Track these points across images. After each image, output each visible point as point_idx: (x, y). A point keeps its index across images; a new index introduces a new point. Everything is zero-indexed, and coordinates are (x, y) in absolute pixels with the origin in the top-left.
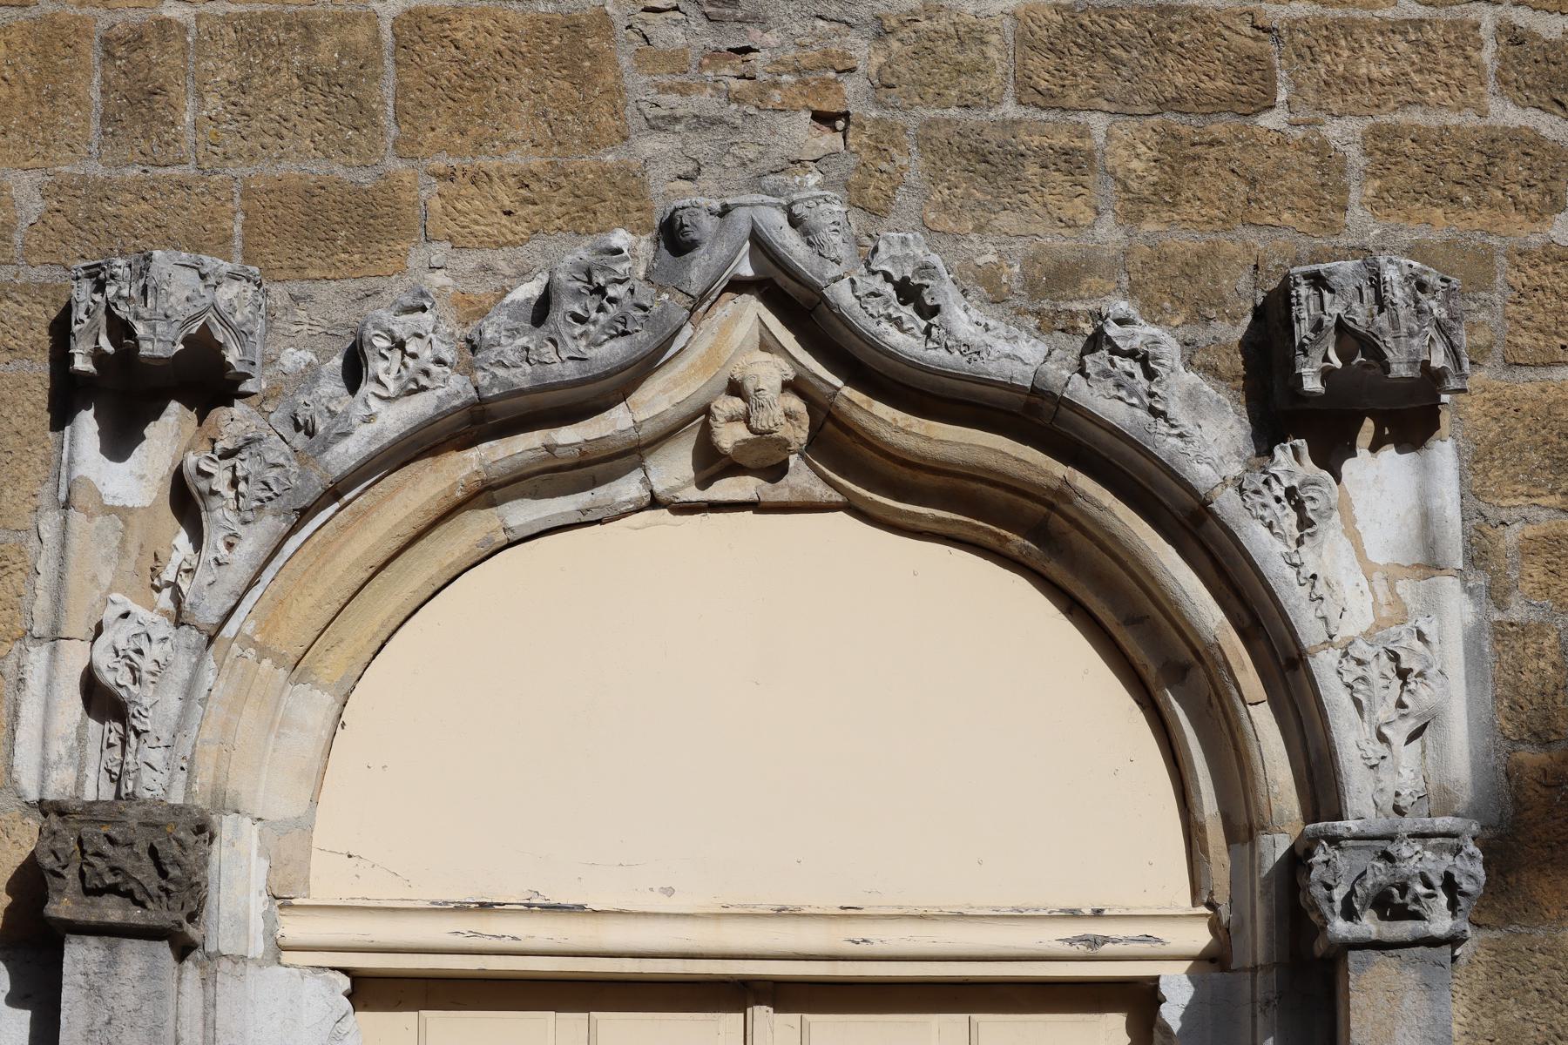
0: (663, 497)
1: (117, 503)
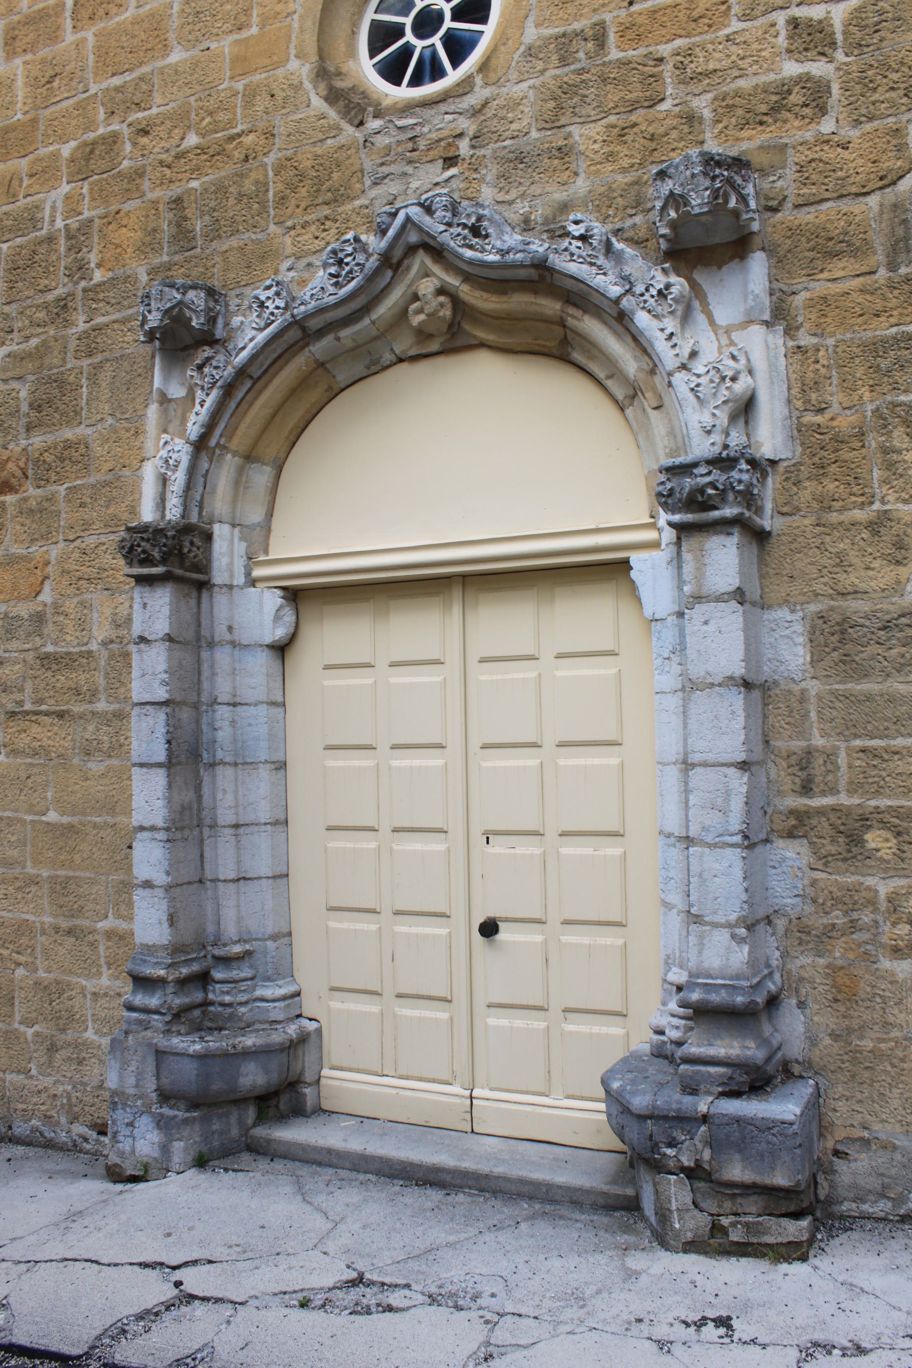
0: (403, 357)
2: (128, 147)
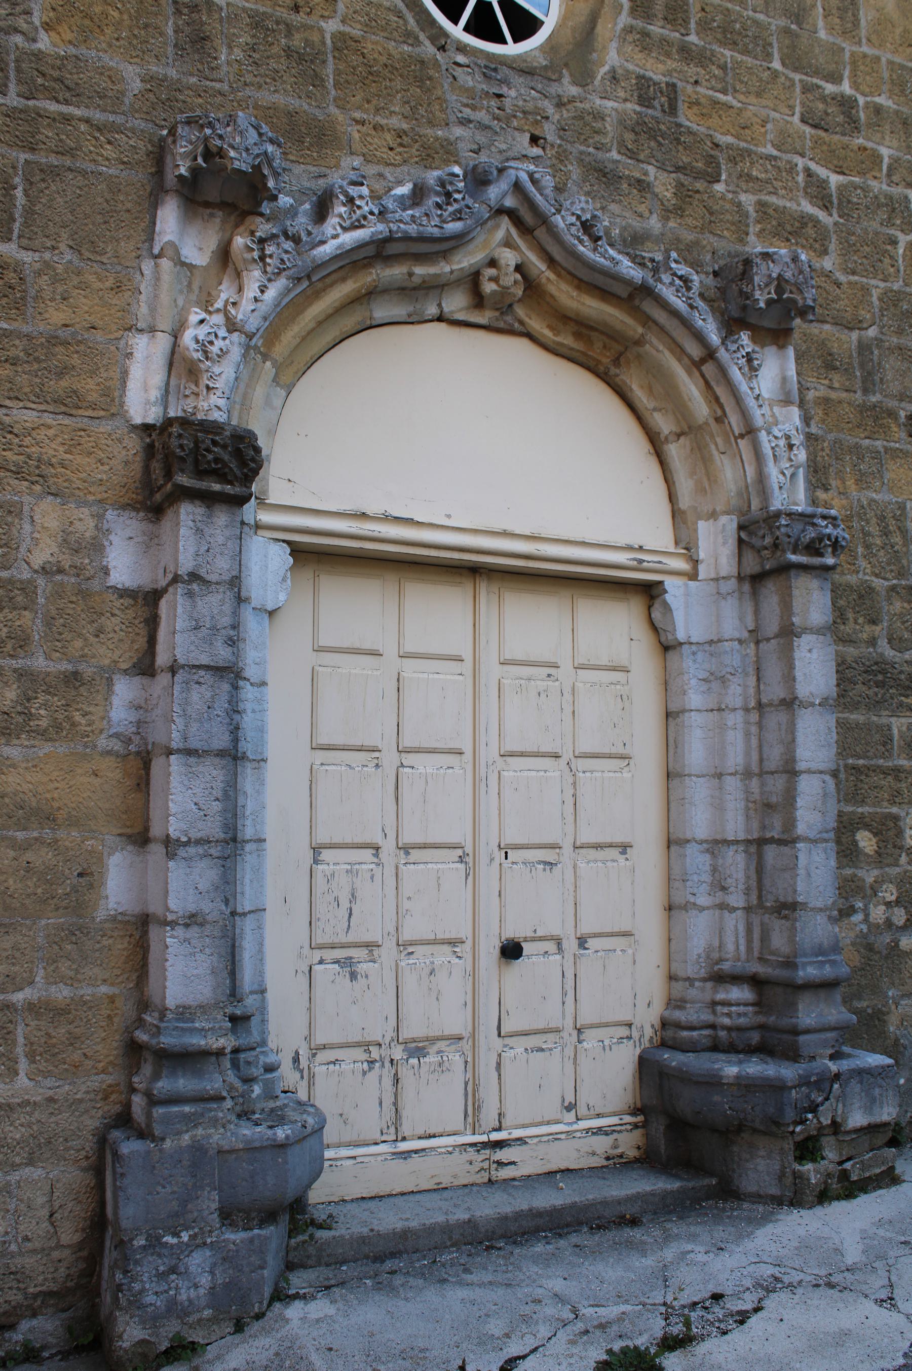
0: (448, 316)
1: (187, 261)
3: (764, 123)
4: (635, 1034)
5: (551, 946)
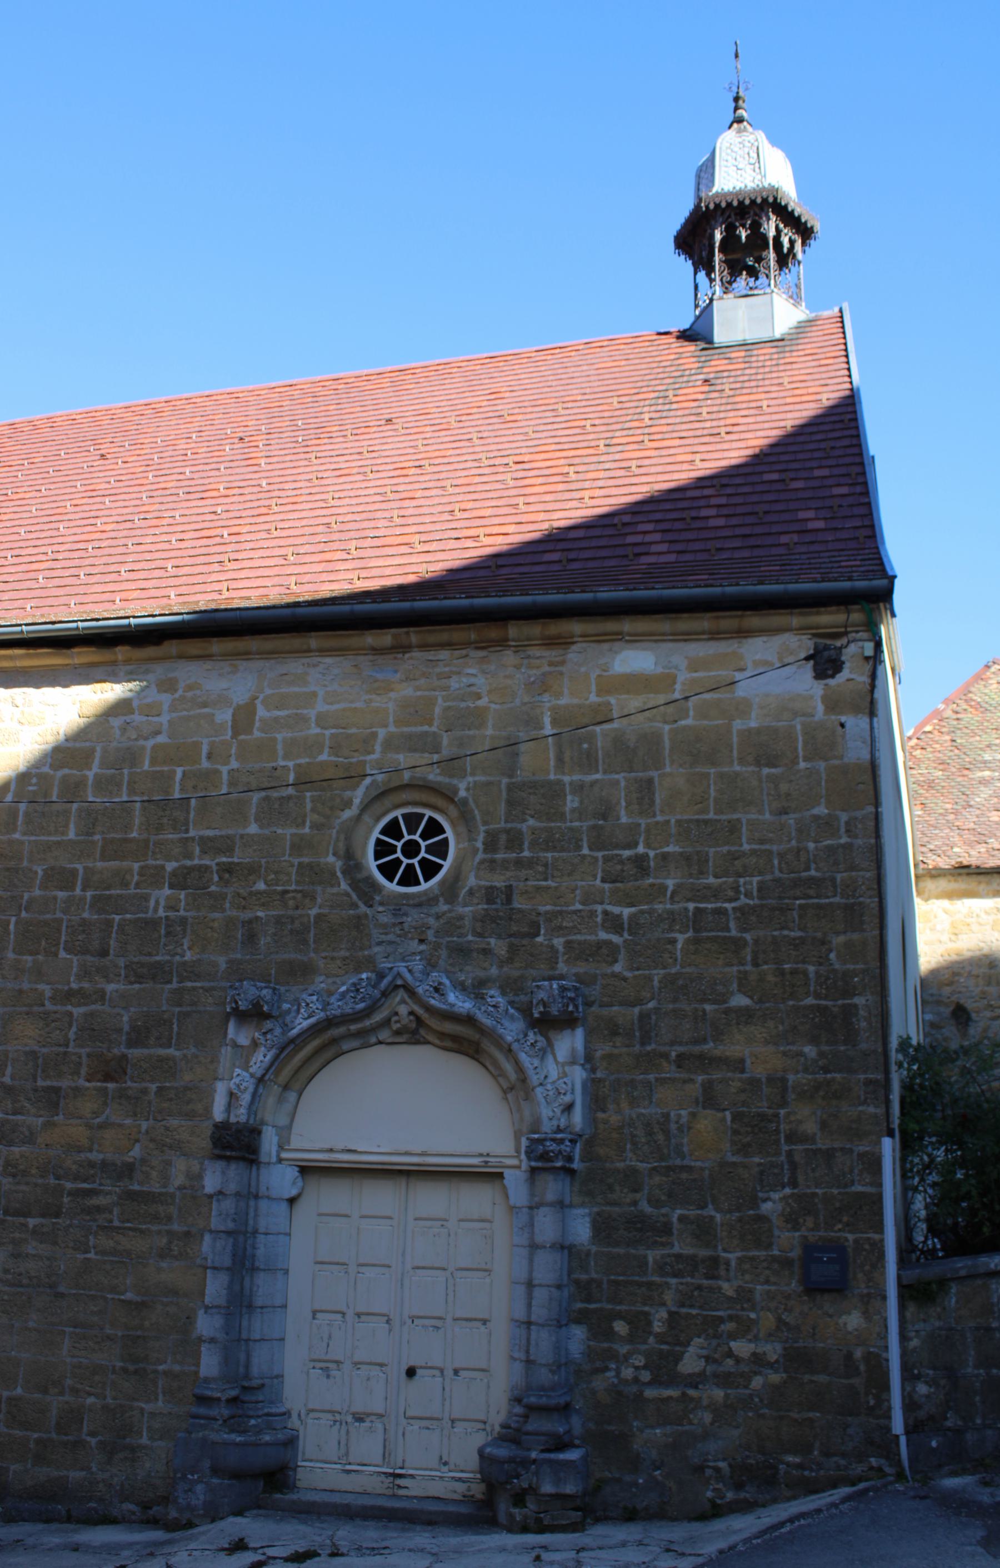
2: (216, 878)
3: (573, 891)
4: (489, 1429)
5: (437, 1373)
